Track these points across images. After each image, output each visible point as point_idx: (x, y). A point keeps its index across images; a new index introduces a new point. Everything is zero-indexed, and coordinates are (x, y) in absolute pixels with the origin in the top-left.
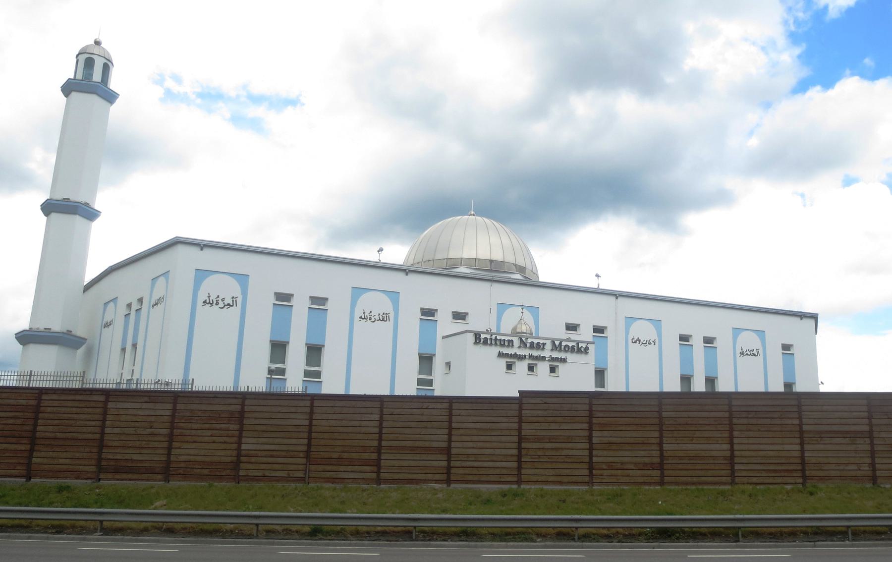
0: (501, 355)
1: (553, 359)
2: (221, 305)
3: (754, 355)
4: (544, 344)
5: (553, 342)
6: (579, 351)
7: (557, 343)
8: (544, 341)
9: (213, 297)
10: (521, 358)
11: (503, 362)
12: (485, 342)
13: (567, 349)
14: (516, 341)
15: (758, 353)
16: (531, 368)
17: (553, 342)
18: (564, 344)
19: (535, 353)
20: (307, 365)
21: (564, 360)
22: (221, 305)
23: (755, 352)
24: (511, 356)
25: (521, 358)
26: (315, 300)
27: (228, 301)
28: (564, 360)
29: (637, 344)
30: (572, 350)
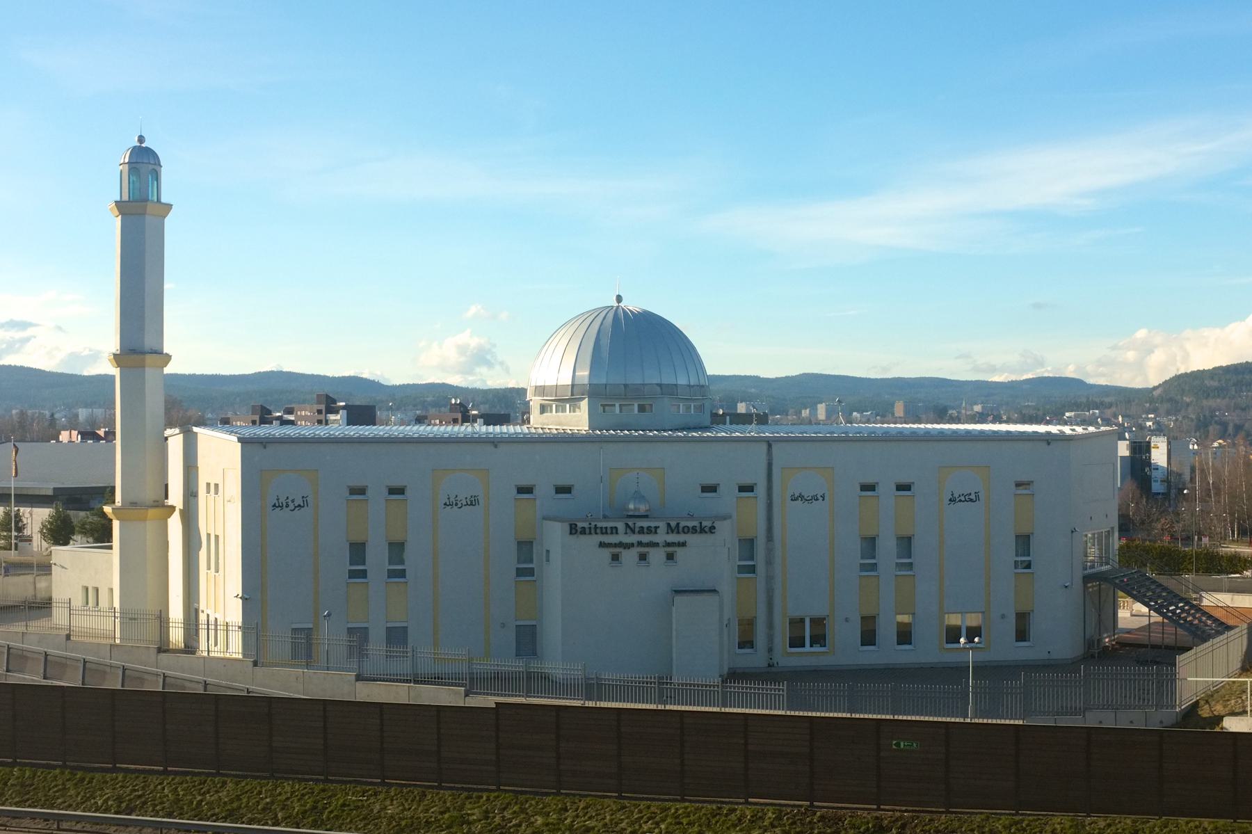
0: (602, 545)
1: (668, 545)
2: (292, 506)
3: (971, 500)
4: (656, 528)
5: (669, 525)
6: (702, 531)
7: (673, 524)
8: (656, 524)
9: (282, 500)
10: (628, 546)
11: (607, 553)
12: (583, 531)
13: (687, 530)
14: (621, 526)
15: (978, 497)
16: (643, 557)
17: (669, 525)
18: (682, 525)
19: (646, 538)
20: (390, 564)
21: (683, 544)
22: (292, 506)
23: (973, 497)
24: (615, 545)
25: (628, 546)
26: (393, 491)
27: (299, 501)
28: (683, 544)
29: (799, 502)
30: (694, 530)
